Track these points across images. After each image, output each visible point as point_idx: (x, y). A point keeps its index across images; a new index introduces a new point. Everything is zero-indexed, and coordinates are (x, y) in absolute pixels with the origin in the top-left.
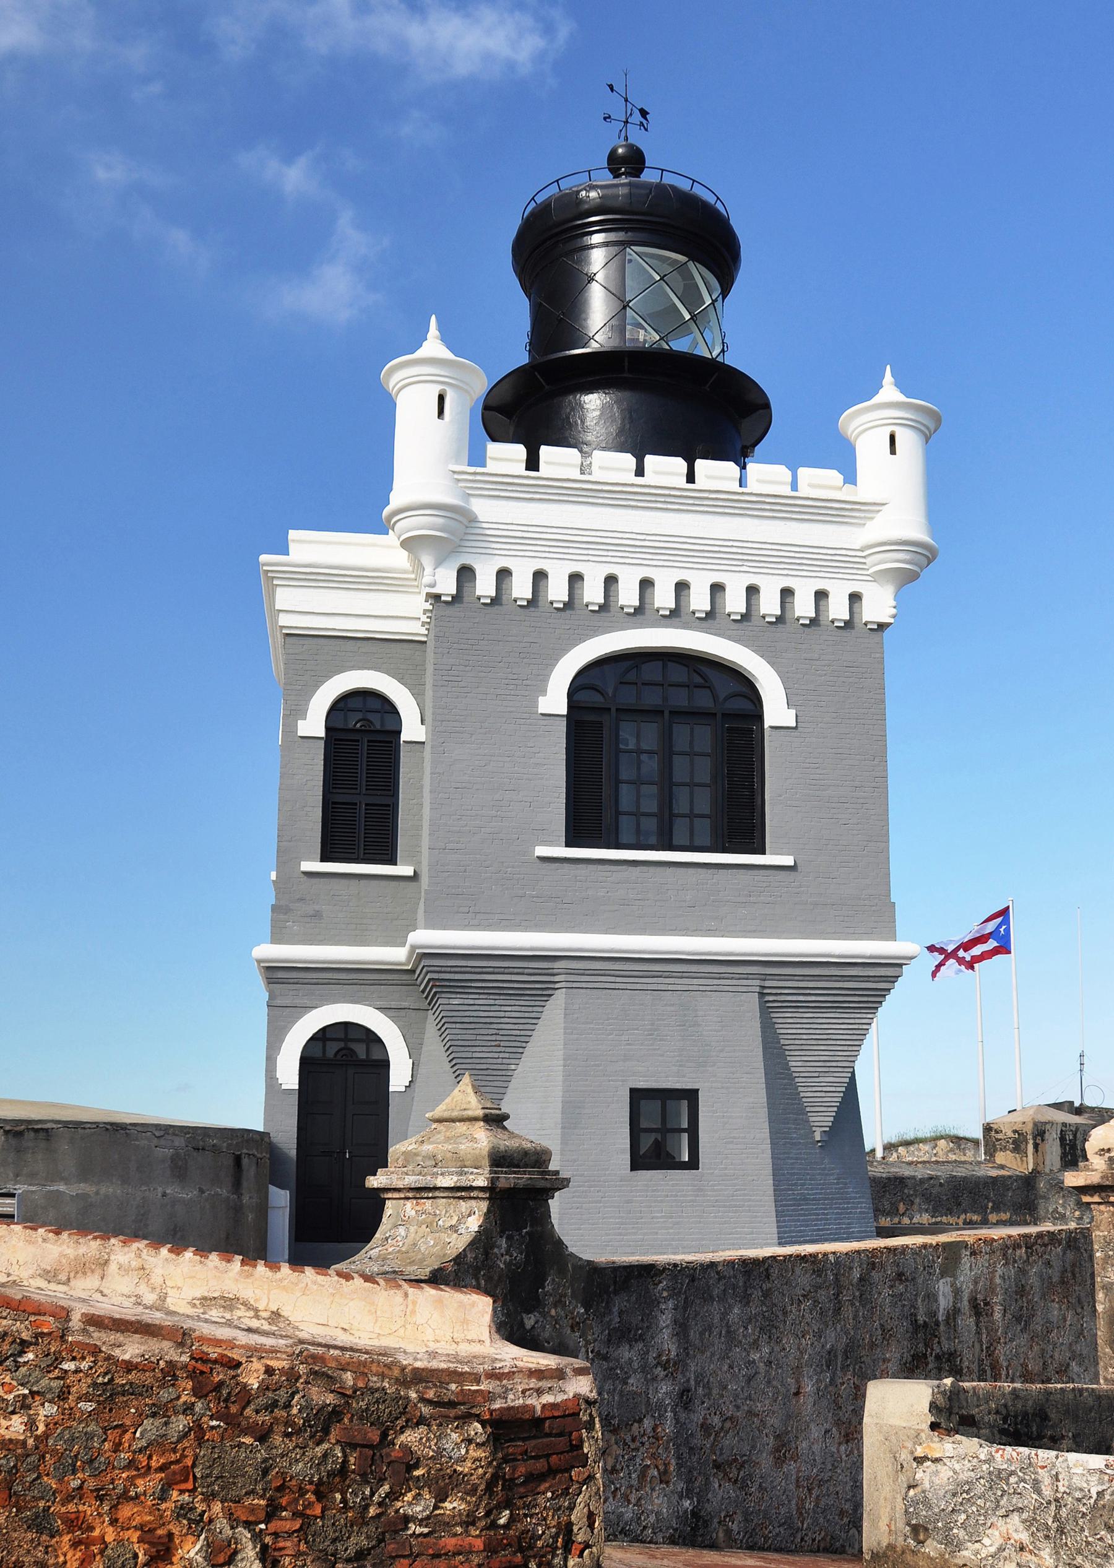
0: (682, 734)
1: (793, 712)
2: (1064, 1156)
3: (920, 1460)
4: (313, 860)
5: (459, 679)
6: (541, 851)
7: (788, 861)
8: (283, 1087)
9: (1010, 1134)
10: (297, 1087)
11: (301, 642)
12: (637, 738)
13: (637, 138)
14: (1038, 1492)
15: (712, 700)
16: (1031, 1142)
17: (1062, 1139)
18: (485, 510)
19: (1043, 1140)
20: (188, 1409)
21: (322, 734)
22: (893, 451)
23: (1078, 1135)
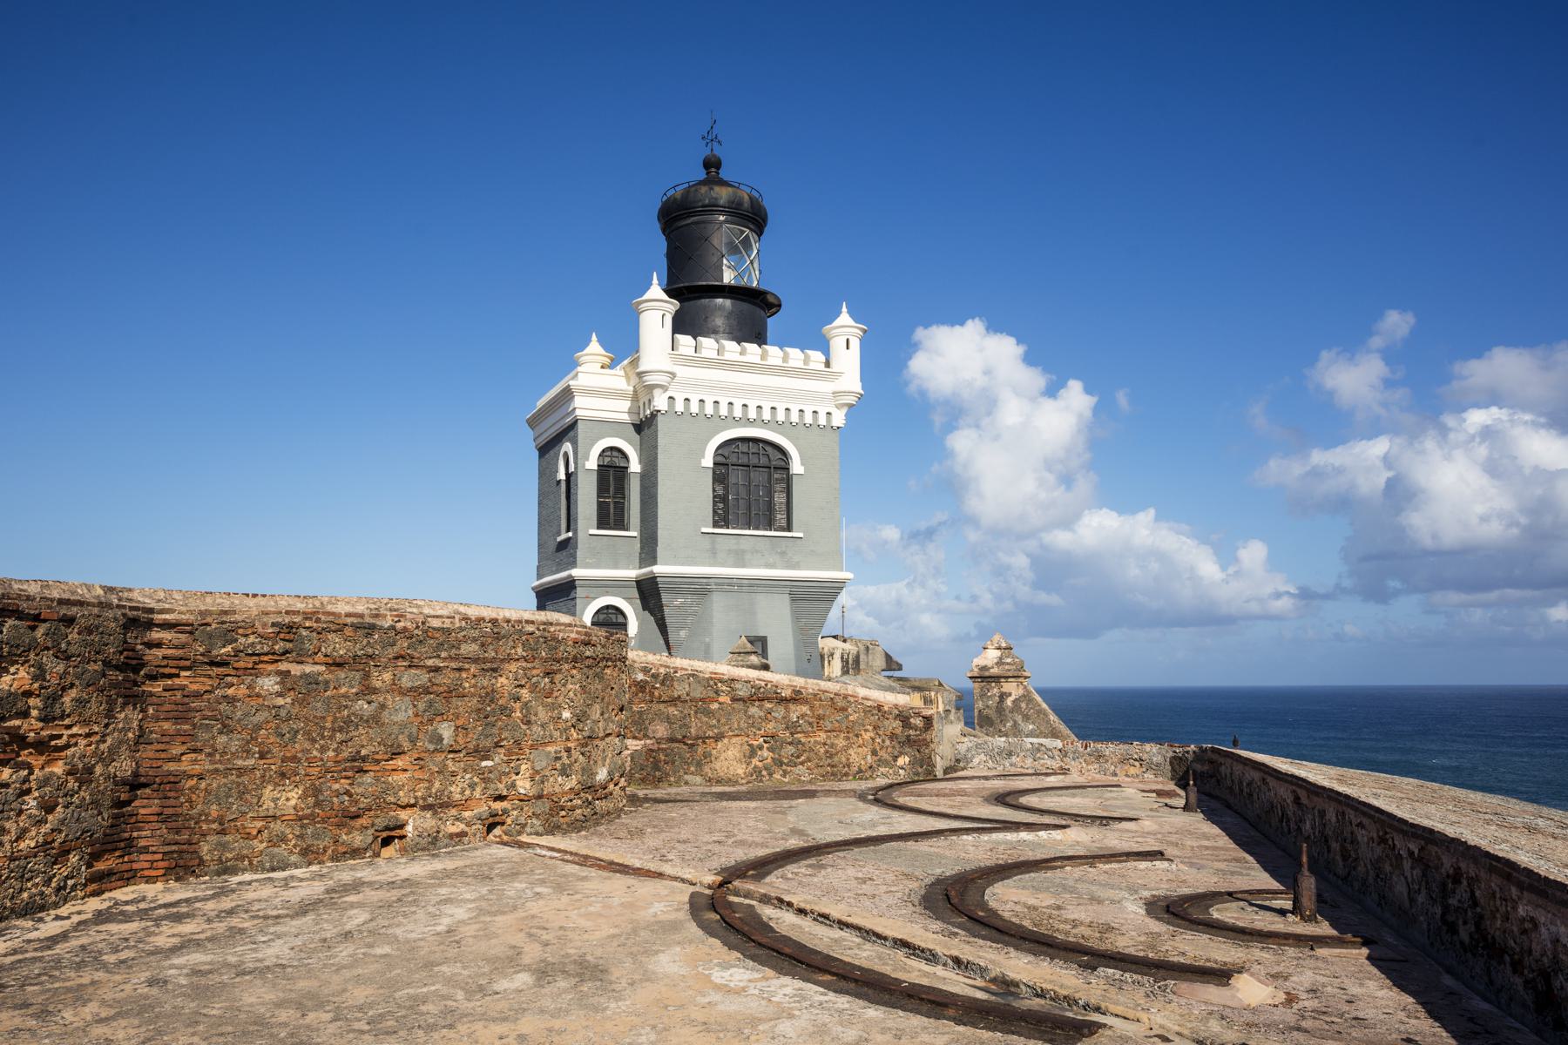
6: (704, 530)
12: (737, 477)
13: (718, 151)
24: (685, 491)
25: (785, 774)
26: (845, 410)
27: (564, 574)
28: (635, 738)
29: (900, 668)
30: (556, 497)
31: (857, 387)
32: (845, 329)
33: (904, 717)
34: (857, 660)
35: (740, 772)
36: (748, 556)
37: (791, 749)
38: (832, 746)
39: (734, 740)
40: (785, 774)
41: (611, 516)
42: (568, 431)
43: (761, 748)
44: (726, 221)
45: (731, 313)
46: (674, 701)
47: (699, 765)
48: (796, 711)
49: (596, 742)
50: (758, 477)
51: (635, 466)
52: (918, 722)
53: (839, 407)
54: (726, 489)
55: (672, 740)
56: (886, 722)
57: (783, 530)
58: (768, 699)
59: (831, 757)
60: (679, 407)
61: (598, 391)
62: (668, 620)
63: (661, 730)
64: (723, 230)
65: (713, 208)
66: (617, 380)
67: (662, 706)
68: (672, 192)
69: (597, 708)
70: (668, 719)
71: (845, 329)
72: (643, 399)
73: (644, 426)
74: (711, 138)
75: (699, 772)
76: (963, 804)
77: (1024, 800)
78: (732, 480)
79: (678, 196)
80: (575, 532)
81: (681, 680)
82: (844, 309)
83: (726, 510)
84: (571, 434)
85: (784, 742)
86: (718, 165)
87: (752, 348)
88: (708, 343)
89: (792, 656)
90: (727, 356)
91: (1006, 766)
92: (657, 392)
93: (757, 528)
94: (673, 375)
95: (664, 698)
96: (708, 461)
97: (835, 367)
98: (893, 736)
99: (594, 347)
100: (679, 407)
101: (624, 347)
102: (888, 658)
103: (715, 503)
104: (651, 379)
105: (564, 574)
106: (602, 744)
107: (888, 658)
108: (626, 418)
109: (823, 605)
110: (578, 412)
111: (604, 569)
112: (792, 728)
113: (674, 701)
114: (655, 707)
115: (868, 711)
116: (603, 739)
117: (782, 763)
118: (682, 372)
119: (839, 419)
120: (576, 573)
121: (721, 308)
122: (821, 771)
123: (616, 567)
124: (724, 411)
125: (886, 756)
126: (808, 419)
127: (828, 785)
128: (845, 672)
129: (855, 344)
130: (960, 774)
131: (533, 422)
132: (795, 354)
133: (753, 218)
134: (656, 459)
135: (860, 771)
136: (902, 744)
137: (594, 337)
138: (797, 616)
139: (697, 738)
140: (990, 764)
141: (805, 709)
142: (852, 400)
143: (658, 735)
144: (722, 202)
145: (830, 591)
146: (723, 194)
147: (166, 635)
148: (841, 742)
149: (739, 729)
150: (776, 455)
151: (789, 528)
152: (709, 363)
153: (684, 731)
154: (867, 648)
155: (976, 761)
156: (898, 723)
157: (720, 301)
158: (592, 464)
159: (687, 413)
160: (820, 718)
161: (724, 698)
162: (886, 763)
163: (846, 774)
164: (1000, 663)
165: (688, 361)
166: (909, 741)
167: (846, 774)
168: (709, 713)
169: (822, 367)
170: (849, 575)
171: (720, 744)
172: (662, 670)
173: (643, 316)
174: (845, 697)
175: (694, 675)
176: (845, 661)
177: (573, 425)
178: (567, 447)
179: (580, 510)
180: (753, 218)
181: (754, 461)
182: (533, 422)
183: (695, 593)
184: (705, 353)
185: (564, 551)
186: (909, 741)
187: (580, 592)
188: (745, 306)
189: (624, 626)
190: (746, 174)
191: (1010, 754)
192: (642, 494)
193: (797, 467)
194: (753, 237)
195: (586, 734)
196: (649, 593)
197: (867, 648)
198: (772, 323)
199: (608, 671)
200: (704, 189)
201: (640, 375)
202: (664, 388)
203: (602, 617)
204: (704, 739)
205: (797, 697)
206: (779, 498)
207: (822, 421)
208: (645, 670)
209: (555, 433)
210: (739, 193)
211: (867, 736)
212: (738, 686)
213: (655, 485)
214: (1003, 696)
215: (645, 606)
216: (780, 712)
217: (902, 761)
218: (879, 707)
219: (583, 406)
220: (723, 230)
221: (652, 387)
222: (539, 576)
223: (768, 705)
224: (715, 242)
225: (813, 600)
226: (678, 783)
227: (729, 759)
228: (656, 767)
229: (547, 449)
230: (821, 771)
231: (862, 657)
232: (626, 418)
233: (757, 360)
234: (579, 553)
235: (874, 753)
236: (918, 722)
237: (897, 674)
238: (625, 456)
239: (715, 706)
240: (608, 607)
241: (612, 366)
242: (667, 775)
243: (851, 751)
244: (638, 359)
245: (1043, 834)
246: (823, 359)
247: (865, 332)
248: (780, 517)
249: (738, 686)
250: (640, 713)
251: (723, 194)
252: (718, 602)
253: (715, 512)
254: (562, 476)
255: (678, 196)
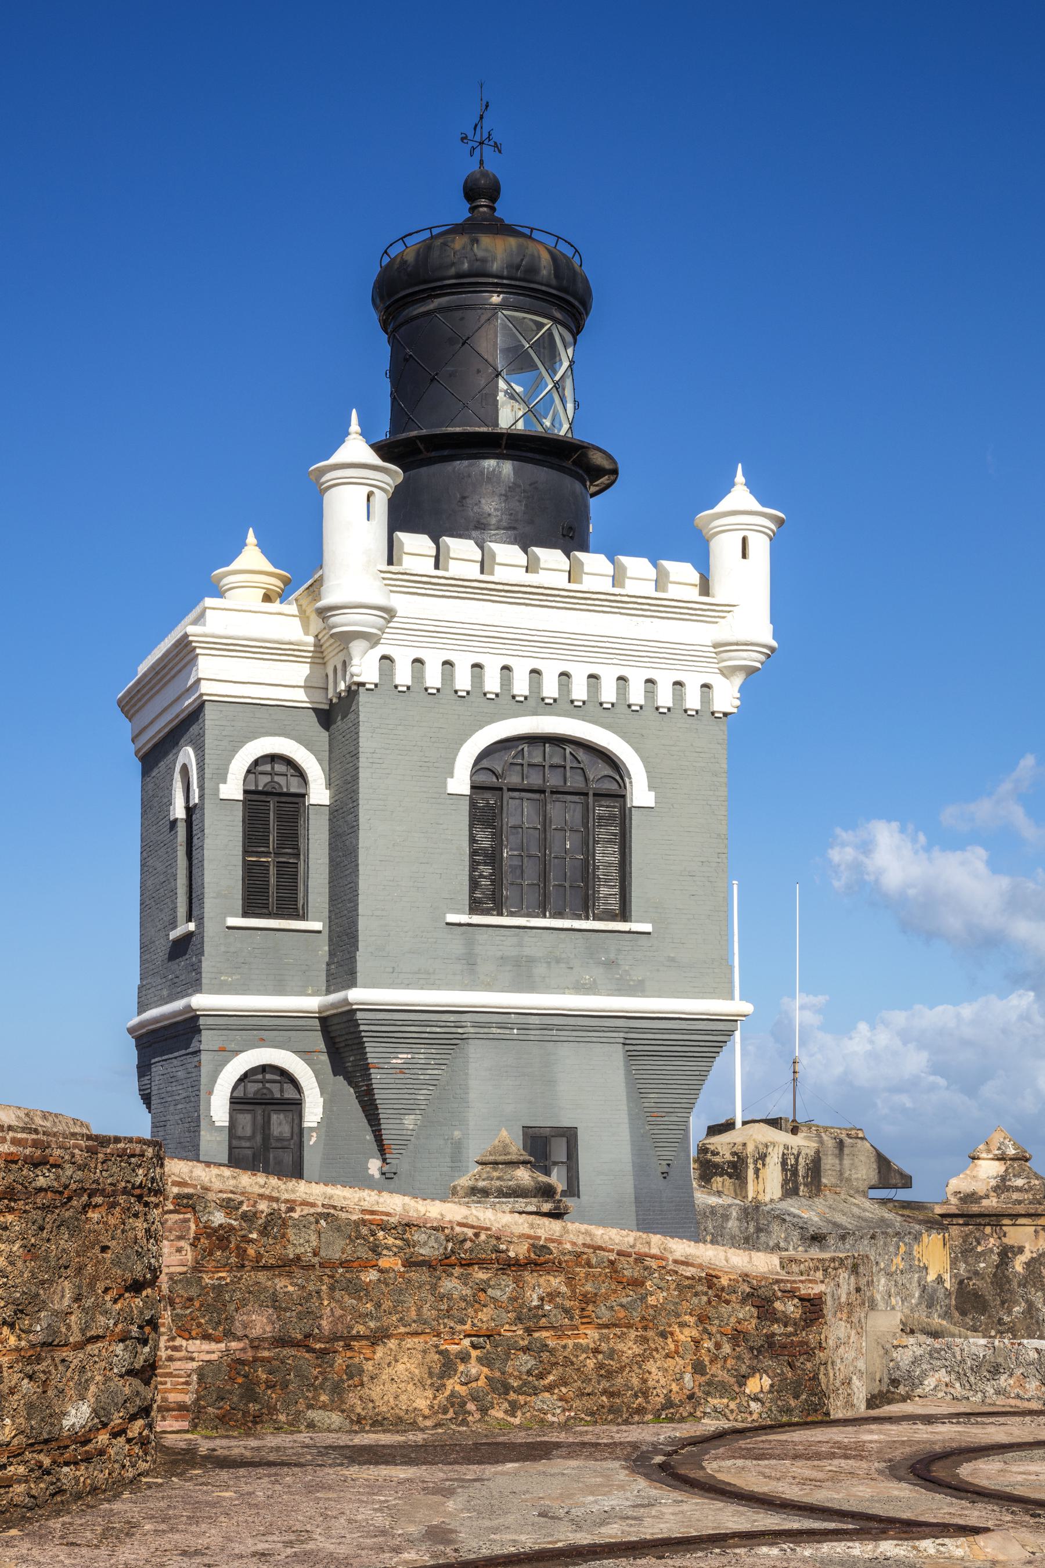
0: (555, 810)
1: (653, 794)
2: (785, 1182)
3: (896, 1347)
4: (236, 916)
5: (381, 761)
6: (452, 918)
7: (647, 927)
8: (217, 1124)
9: (728, 1157)
10: (227, 1124)
11: (220, 708)
12: (520, 813)
13: (495, 165)
14: (955, 1357)
15: (582, 779)
16: (751, 1166)
17: (784, 1163)
18: (405, 605)
19: (764, 1165)
20: (706, 1294)
21: (241, 797)
22: (744, 555)
23: (800, 1159)
24: (412, 840)
25: (514, 1408)
26: (738, 680)
27: (178, 1005)
28: (206, 1337)
29: (906, 1182)
30: (170, 846)
31: (764, 634)
32: (741, 521)
33: (760, 1298)
34: (815, 1167)
35: (422, 1404)
36: (540, 970)
37: (526, 1361)
38: (612, 1354)
39: (410, 1342)
40: (514, 1408)
41: (270, 889)
42: (188, 724)
43: (465, 1358)
44: (503, 306)
45: (512, 488)
46: (286, 1266)
47: (337, 1390)
48: (536, 1288)
49: (65, 1353)
50: (563, 813)
51: (319, 794)
52: (790, 1308)
53: (727, 672)
54: (497, 837)
55: (281, 1341)
56: (724, 1309)
57: (612, 917)
58: (482, 1263)
59: (610, 1375)
60: (403, 676)
61: (245, 643)
62: (379, 1095)
63: (260, 1323)
64: (499, 325)
65: (477, 279)
66: (286, 624)
67: (262, 1276)
68: (394, 252)
69: (67, 1288)
70: (275, 1302)
71: (741, 521)
72: (334, 660)
73: (335, 714)
74: (481, 141)
75: (338, 1403)
76: (835, 1478)
77: (967, 1471)
78: (510, 820)
79: (410, 257)
80: (200, 925)
81: (302, 1225)
82: (740, 478)
83: (497, 880)
84: (194, 729)
85: (511, 1348)
86: (493, 192)
87: (552, 558)
88: (462, 550)
89: (629, 1168)
90: (500, 574)
91: (987, 1393)
92: (357, 647)
93: (559, 914)
94: (389, 613)
95: (268, 1260)
96: (460, 783)
97: (721, 593)
98: (737, 1337)
99: (252, 556)
100: (403, 676)
101: (301, 563)
102: (883, 1162)
103: (473, 865)
104: (345, 622)
105: (178, 1005)
106: (75, 1358)
107: (883, 1162)
108: (300, 697)
109: (693, 1065)
110: (205, 688)
111: (257, 999)
112: (530, 1319)
113: (286, 1266)
114: (249, 1277)
115: (686, 1287)
116: (79, 1346)
117: (507, 1389)
118: (405, 605)
119: (727, 697)
120: (200, 1001)
121: (493, 477)
122: (589, 1403)
123: (280, 990)
124: (492, 683)
125: (723, 1376)
126: (665, 698)
127: (591, 1433)
128: (790, 1190)
129: (760, 546)
130: (907, 1408)
131: (130, 705)
132: (637, 567)
133: (565, 298)
134: (355, 779)
135: (669, 1404)
136: (757, 1352)
137: (251, 538)
138: (637, 1090)
139: (335, 1338)
140: (958, 1390)
141: (556, 1282)
142: (753, 659)
143: (256, 1332)
144: (495, 267)
145: (707, 1040)
146: (497, 251)
147: (338, 1027)
148: (629, 1348)
149: (421, 1320)
150: (598, 770)
151: (624, 915)
152: (462, 589)
153: (306, 1324)
154: (841, 1145)
155: (930, 1382)
156: (748, 1311)
157: (490, 464)
158: (233, 789)
159: (418, 687)
160: (587, 1300)
161: (390, 1262)
162: (723, 1389)
163: (640, 1411)
164: (1002, 1187)
165: (419, 586)
166: (770, 1346)
167: (640, 1411)
168: (358, 1290)
169: (693, 594)
170: (747, 1008)
171: (380, 1352)
172: (263, 1206)
173: (328, 497)
174: (640, 1258)
175: (329, 1215)
176: (789, 1171)
177: (197, 713)
178: (187, 755)
179: (207, 879)
180: (565, 298)
181: (554, 780)
182: (130, 705)
183: (432, 1041)
184: (455, 569)
185: (176, 958)
186: (770, 1346)
187: (208, 1040)
188: (542, 474)
189: (295, 1106)
190: (548, 210)
191: (995, 1371)
192: (333, 847)
193: (641, 794)
194: (559, 334)
195: (41, 1338)
196: (343, 1040)
197: (841, 1145)
198: (600, 508)
199: (94, 1215)
200: (459, 242)
201: (324, 613)
202: (372, 640)
203: (252, 1088)
204: (348, 1340)
205: (540, 1259)
206: (605, 856)
207: (693, 700)
208: (229, 1206)
209: (169, 727)
210: (532, 247)
211: (684, 1336)
212: (419, 1236)
213: (354, 829)
214: (1007, 1253)
215: (338, 1067)
216: (504, 1288)
217: (756, 1385)
218: (711, 1280)
219: (216, 676)
220: (499, 325)
221: (346, 639)
222: (142, 1008)
223: (481, 1275)
224: (483, 346)
225: (671, 1057)
226: (293, 1426)
227: (399, 1379)
228: (250, 1393)
229: (155, 757)
230: (589, 1403)
231: (829, 1162)
232: (300, 697)
233: (560, 580)
234: (206, 965)
235: (699, 1368)
236: (790, 1308)
237: (902, 1195)
238: (300, 773)
239: (372, 1276)
240: (264, 1069)
241: (282, 597)
242: (272, 1410)
243: (651, 1366)
244: (320, 581)
245: (928, 1546)
246: (695, 577)
247: (780, 522)
248: (607, 893)
249: (419, 1236)
250: (219, 1289)
251: (497, 251)
252: (479, 1061)
253: (474, 884)
254: (179, 811)
255: (410, 257)
